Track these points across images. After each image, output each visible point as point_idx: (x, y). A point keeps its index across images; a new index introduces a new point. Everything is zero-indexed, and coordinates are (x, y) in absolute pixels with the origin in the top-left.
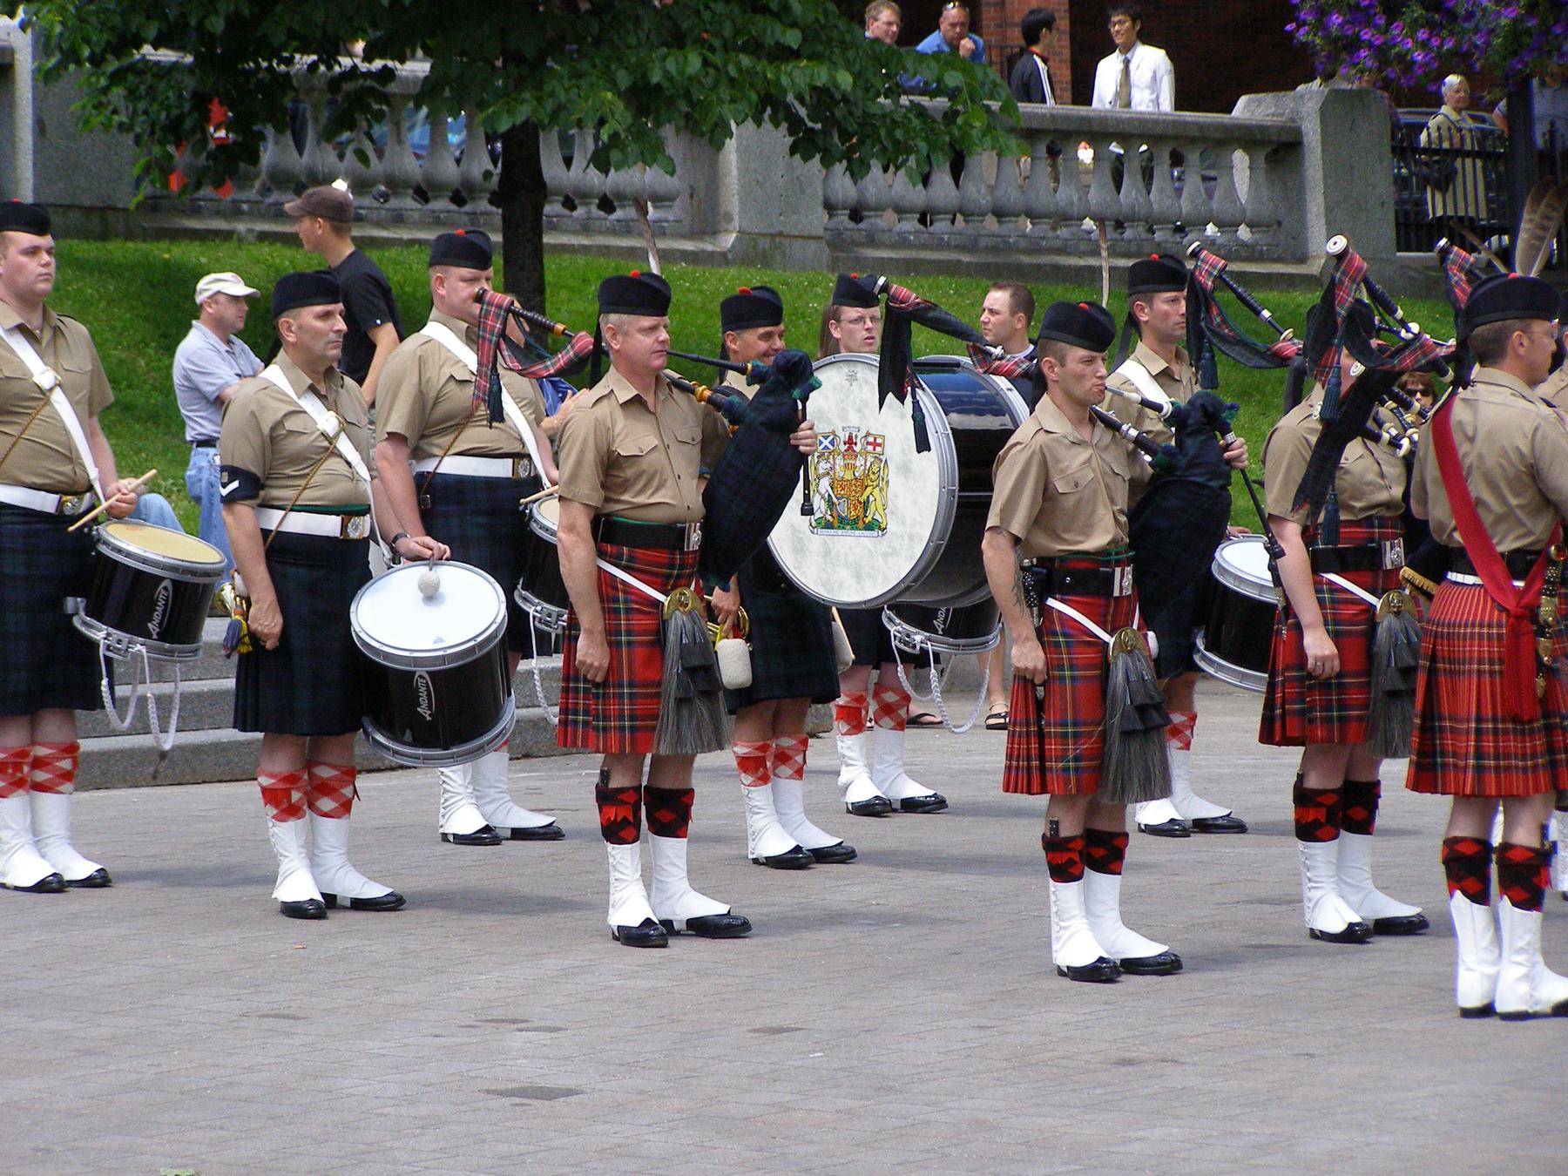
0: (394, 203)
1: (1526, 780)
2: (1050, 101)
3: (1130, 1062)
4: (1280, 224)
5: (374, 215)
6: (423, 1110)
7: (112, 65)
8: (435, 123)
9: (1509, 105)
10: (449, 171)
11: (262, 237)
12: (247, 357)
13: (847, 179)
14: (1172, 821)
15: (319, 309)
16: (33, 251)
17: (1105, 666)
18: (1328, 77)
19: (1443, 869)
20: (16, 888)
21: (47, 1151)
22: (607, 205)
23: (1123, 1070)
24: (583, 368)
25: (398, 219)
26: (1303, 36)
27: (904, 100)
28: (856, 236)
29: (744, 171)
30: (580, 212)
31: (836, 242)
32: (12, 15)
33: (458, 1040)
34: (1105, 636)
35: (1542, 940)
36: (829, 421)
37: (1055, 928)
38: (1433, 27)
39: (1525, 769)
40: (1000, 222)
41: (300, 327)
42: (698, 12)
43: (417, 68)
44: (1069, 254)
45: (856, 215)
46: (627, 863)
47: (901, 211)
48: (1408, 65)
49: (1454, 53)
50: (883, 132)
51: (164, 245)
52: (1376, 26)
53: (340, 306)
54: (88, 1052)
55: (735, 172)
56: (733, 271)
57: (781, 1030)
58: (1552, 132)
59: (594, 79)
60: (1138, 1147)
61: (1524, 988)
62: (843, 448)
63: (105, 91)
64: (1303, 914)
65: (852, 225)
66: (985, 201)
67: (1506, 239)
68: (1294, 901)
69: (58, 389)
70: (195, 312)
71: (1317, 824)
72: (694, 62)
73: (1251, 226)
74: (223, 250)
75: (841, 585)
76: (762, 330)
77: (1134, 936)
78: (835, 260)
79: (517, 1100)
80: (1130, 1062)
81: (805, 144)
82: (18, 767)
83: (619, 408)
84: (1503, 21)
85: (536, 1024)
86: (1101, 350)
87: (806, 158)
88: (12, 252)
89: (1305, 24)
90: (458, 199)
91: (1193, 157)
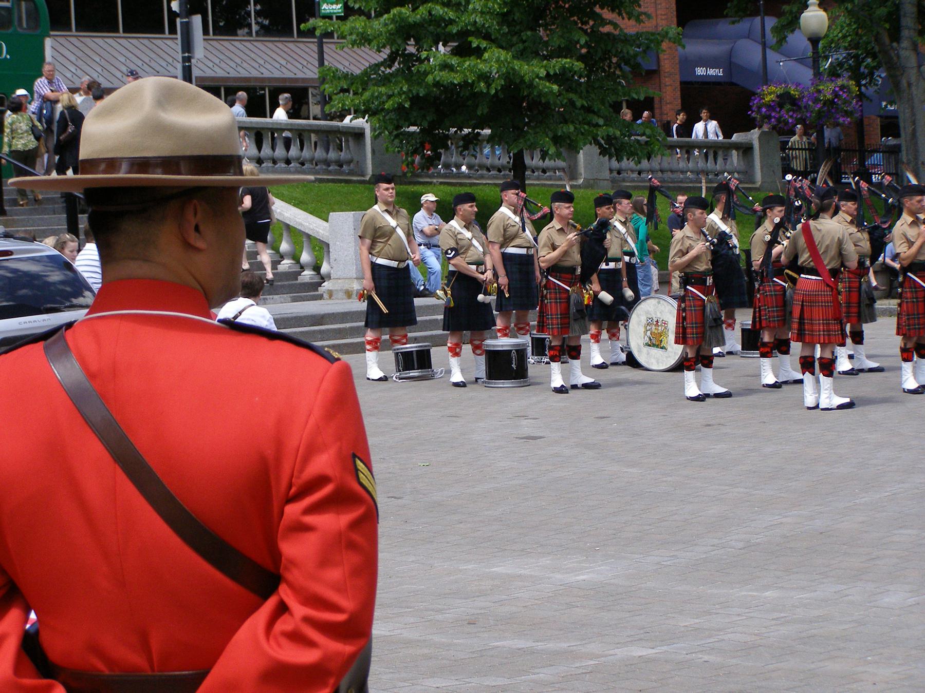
0: (480, 172)
1: (836, 338)
2: (675, 137)
3: (709, 425)
4: (747, 172)
5: (474, 176)
6: (497, 444)
7: (395, 133)
8: (493, 147)
9: (817, 135)
10: (497, 162)
11: (441, 183)
12: (438, 219)
13: (616, 162)
14: (720, 352)
15: (470, 204)
16: (387, 189)
17: (704, 306)
18: (760, 127)
19: (800, 365)
20: (373, 380)
21: (384, 459)
22: (544, 171)
23: (708, 427)
24: (381, 234)
25: (482, 177)
26: (754, 115)
27: (633, 138)
28: (619, 179)
29: (585, 160)
30: (536, 174)
31: (613, 181)
32: (364, 118)
33: (507, 422)
34: (704, 297)
35: (833, 385)
36: (651, 314)
37: (686, 385)
38: (794, 111)
39: (835, 335)
40: (662, 174)
41: (464, 210)
42: (571, 113)
43: (487, 132)
44: (684, 183)
45: (619, 173)
46: (557, 368)
47: (632, 171)
48: (786, 123)
49: (801, 118)
50: (627, 148)
51: (411, 186)
52: (777, 111)
53: (475, 204)
54: (396, 429)
55: (582, 160)
56: (582, 190)
57: (604, 418)
58: (830, 142)
59: (541, 134)
60: (713, 451)
61: (828, 401)
62: (655, 323)
63: (393, 140)
64: (761, 380)
65: (618, 176)
66: (657, 167)
67: (816, 175)
68: (758, 376)
69: (398, 227)
70: (422, 206)
71: (768, 352)
72: (572, 128)
73: (738, 173)
74: (429, 188)
75: (652, 363)
76: (607, 207)
77: (717, 386)
78: (613, 186)
79: (525, 440)
80: (709, 425)
81: (603, 152)
82: (376, 343)
83: (557, 232)
84: (816, 109)
85: (530, 417)
86: (705, 210)
87: (604, 156)
88: (381, 189)
89: (754, 111)
90: (499, 171)
91: (720, 153)
